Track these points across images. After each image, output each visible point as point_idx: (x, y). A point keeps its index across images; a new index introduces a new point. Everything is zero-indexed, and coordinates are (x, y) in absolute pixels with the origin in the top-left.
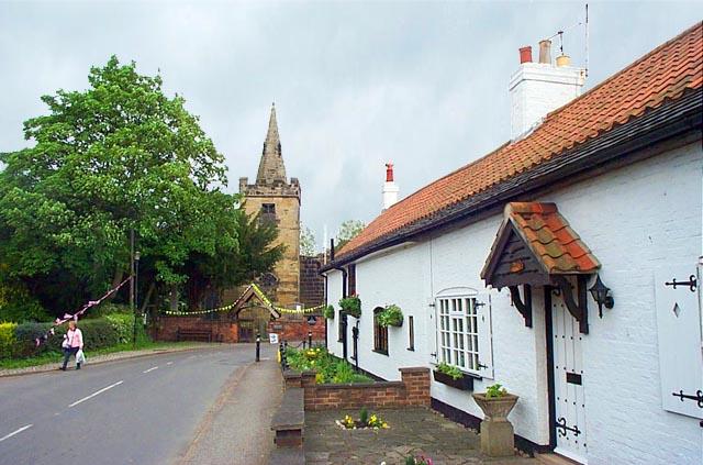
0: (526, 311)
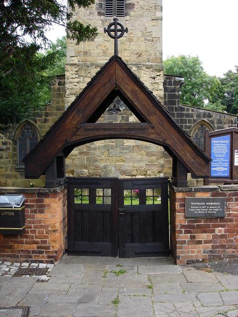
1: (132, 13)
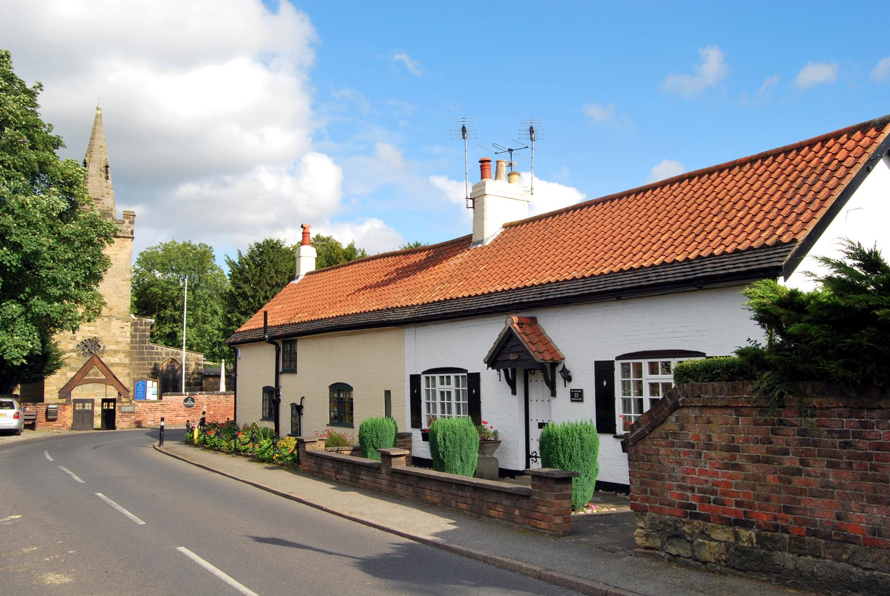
0: (512, 384)
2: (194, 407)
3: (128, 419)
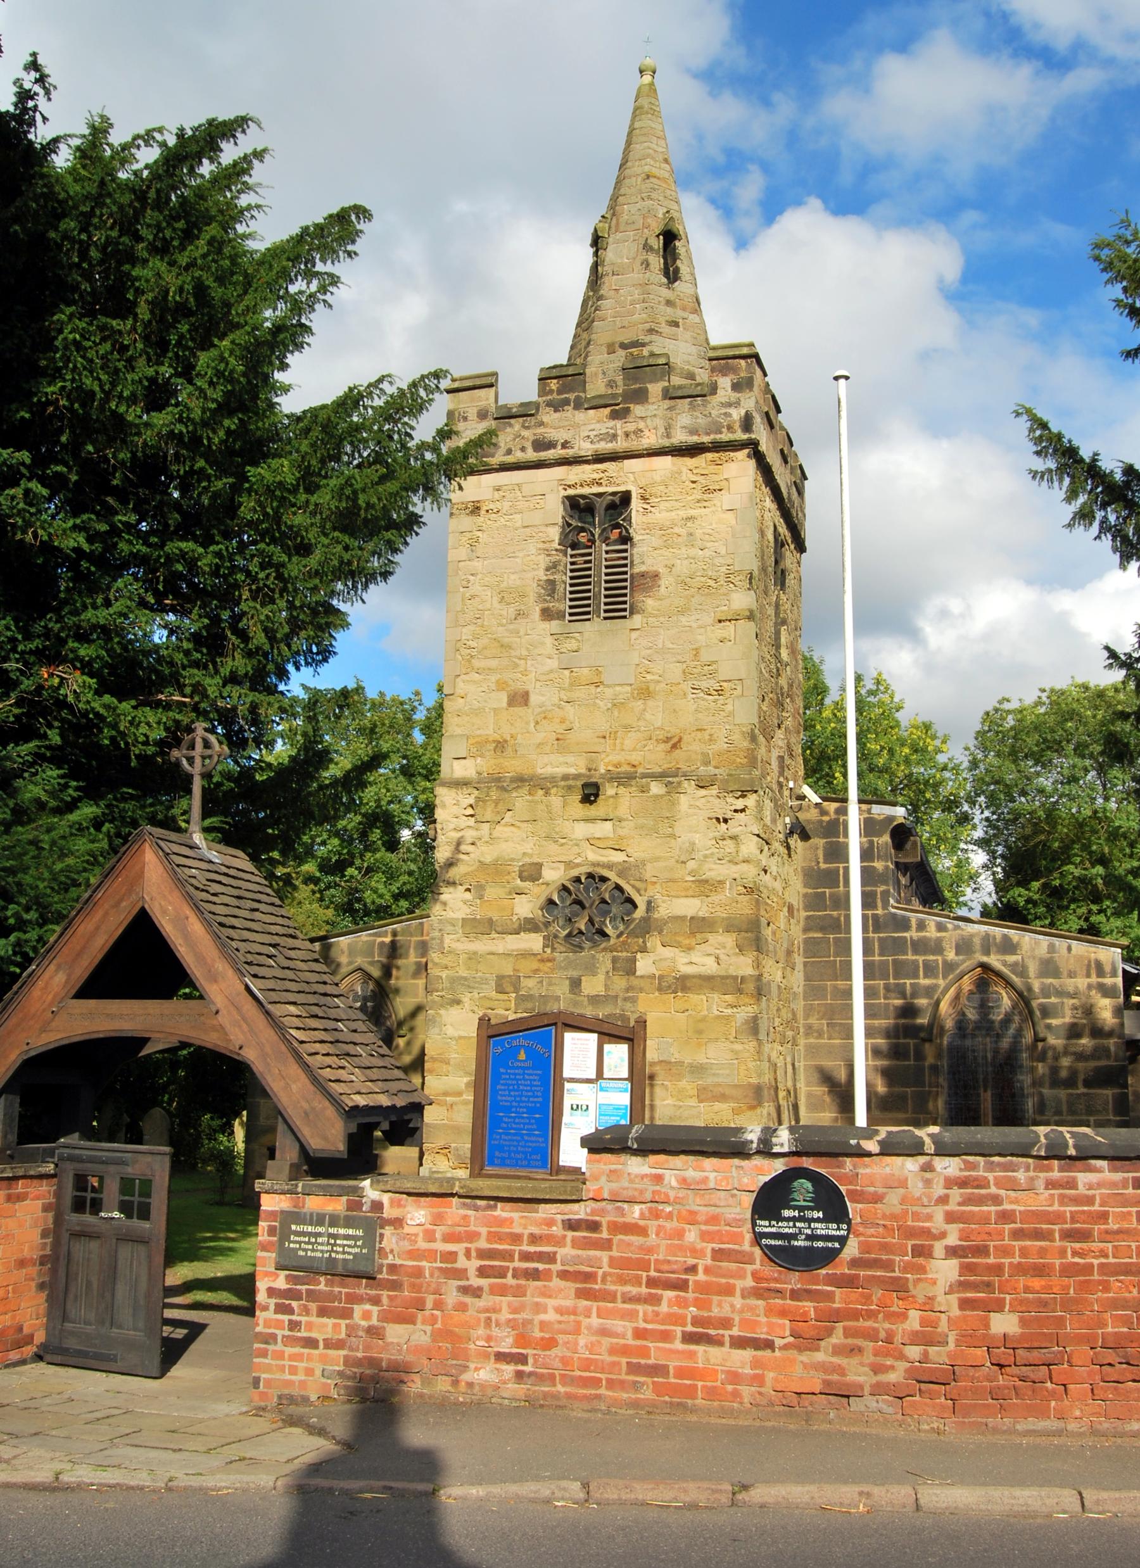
1: (650, 603)
2: (840, 1268)
3: (325, 1328)
